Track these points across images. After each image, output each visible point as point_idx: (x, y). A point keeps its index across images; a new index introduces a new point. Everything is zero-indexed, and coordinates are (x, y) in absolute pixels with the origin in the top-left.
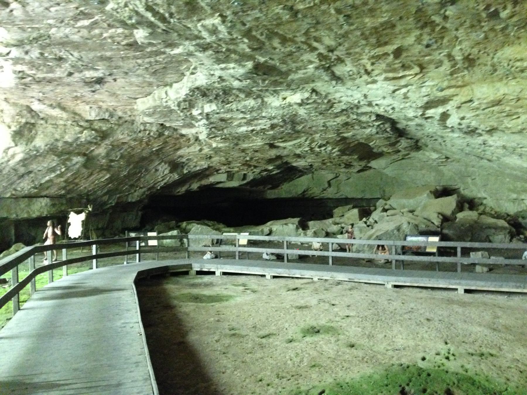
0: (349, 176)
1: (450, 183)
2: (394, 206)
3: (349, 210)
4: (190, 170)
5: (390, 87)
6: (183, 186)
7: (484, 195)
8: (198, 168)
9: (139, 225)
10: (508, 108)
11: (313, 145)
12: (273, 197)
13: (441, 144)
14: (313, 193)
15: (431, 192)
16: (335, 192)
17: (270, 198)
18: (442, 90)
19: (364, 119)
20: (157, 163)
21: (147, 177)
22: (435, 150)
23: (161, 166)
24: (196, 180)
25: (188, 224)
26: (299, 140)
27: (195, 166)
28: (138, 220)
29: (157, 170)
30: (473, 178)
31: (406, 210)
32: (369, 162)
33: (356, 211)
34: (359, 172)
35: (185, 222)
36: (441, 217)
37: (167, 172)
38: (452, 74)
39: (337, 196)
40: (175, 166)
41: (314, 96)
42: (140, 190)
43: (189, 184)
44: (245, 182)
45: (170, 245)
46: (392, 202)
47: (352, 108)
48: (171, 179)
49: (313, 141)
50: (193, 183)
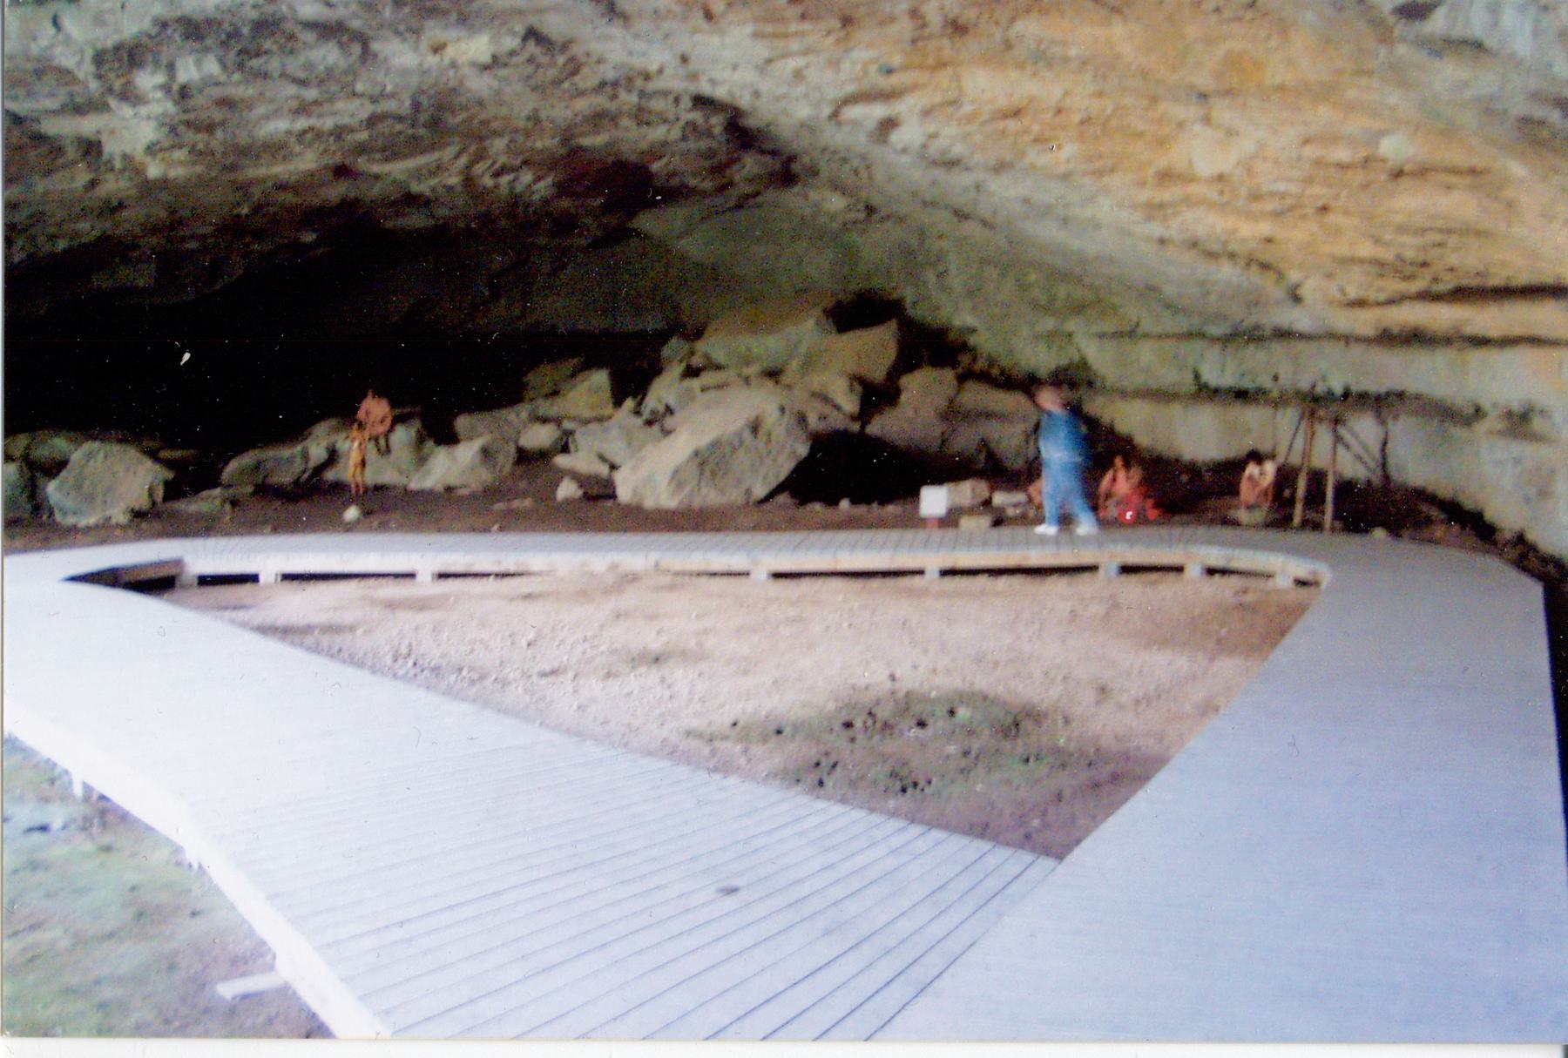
1: (877, 282)
2: (719, 356)
3: (573, 375)
5: (761, 51)
7: (970, 321)
8: (62, 245)
10: (1036, 128)
11: (479, 168)
13: (856, 172)
15: (825, 311)
18: (890, 72)
19: (658, 105)
22: (837, 186)
26: (436, 155)
30: (941, 269)
31: (753, 370)
32: (632, 215)
33: (600, 379)
34: (597, 244)
36: (858, 388)
38: (914, 42)
41: (532, 47)
46: (713, 346)
47: (630, 80)
49: (479, 157)
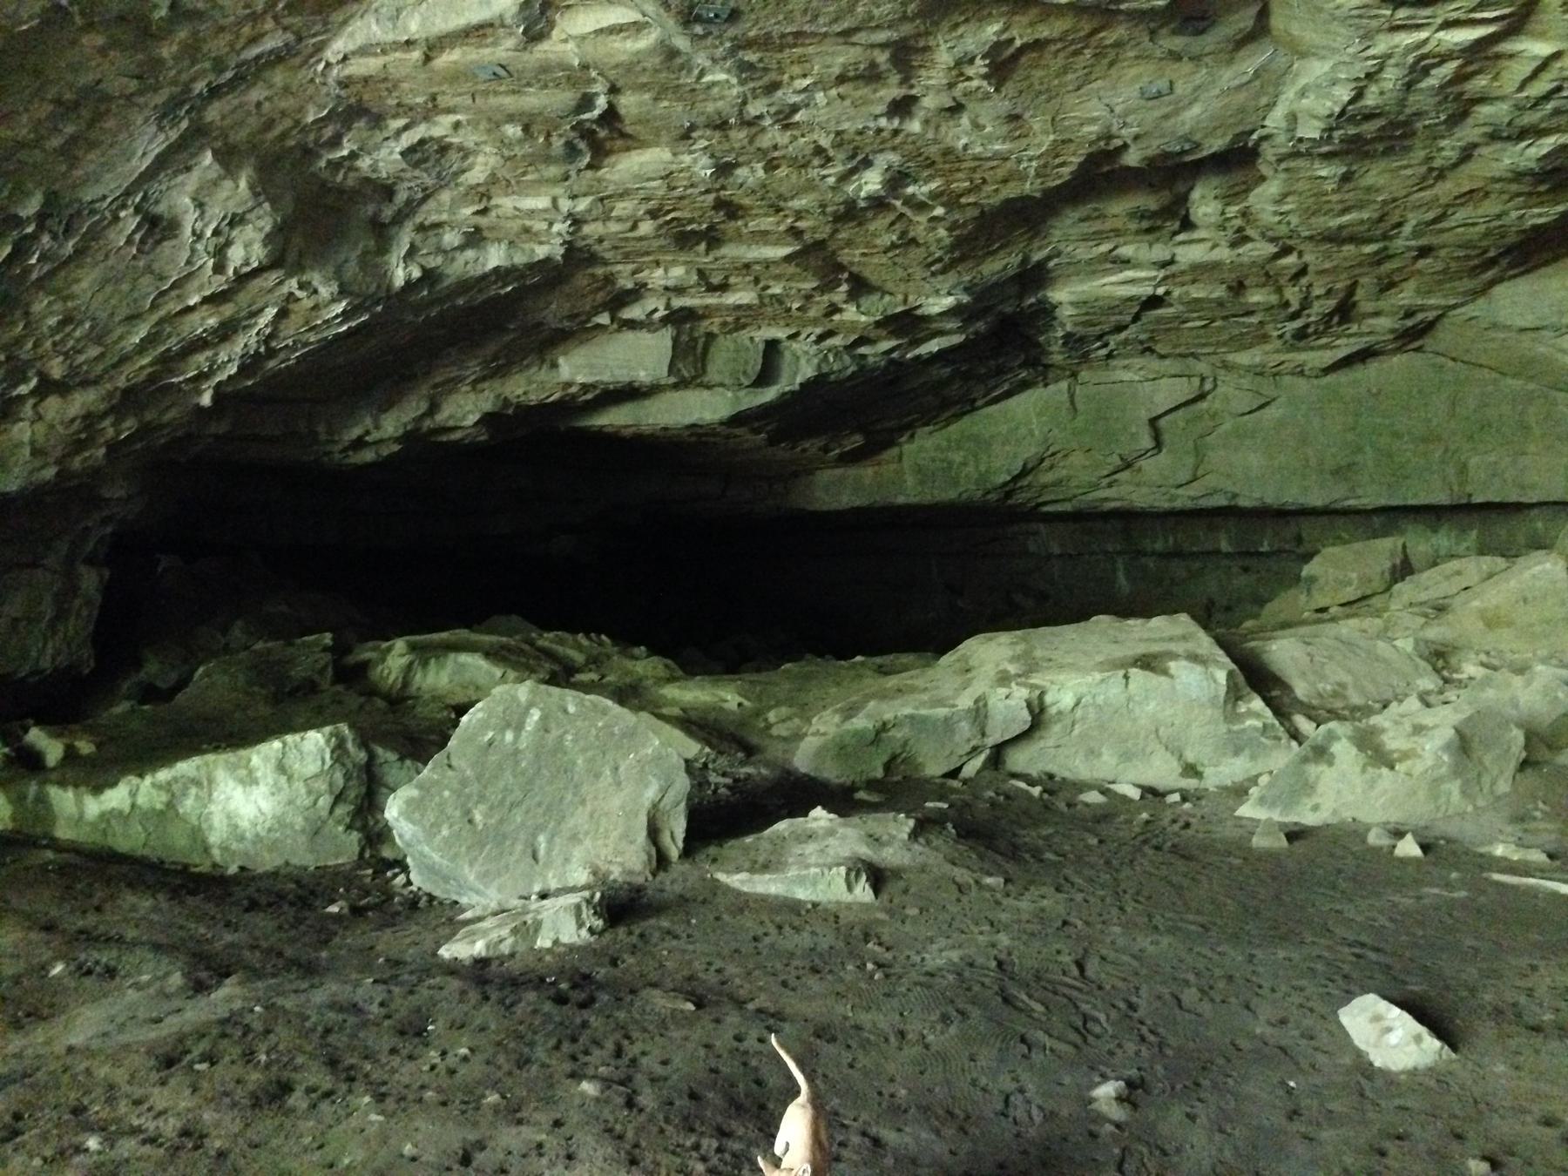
0: (1268, 390)
4: (434, 262)
6: (387, 405)
8: (495, 257)
9: (87, 659)
12: (846, 500)
14: (1058, 483)
16: (1184, 476)
17: (835, 506)
20: (148, 144)
21: (85, 282)
23: (192, 181)
24: (473, 369)
25: (424, 654)
27: (475, 238)
28: (79, 626)
29: (158, 228)
35: (400, 644)
37: (247, 249)
39: (1184, 499)
40: (321, 210)
42: (52, 404)
43: (425, 390)
44: (769, 394)
45: (268, 862)
48: (290, 329)
50: (452, 385)
